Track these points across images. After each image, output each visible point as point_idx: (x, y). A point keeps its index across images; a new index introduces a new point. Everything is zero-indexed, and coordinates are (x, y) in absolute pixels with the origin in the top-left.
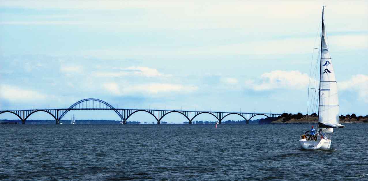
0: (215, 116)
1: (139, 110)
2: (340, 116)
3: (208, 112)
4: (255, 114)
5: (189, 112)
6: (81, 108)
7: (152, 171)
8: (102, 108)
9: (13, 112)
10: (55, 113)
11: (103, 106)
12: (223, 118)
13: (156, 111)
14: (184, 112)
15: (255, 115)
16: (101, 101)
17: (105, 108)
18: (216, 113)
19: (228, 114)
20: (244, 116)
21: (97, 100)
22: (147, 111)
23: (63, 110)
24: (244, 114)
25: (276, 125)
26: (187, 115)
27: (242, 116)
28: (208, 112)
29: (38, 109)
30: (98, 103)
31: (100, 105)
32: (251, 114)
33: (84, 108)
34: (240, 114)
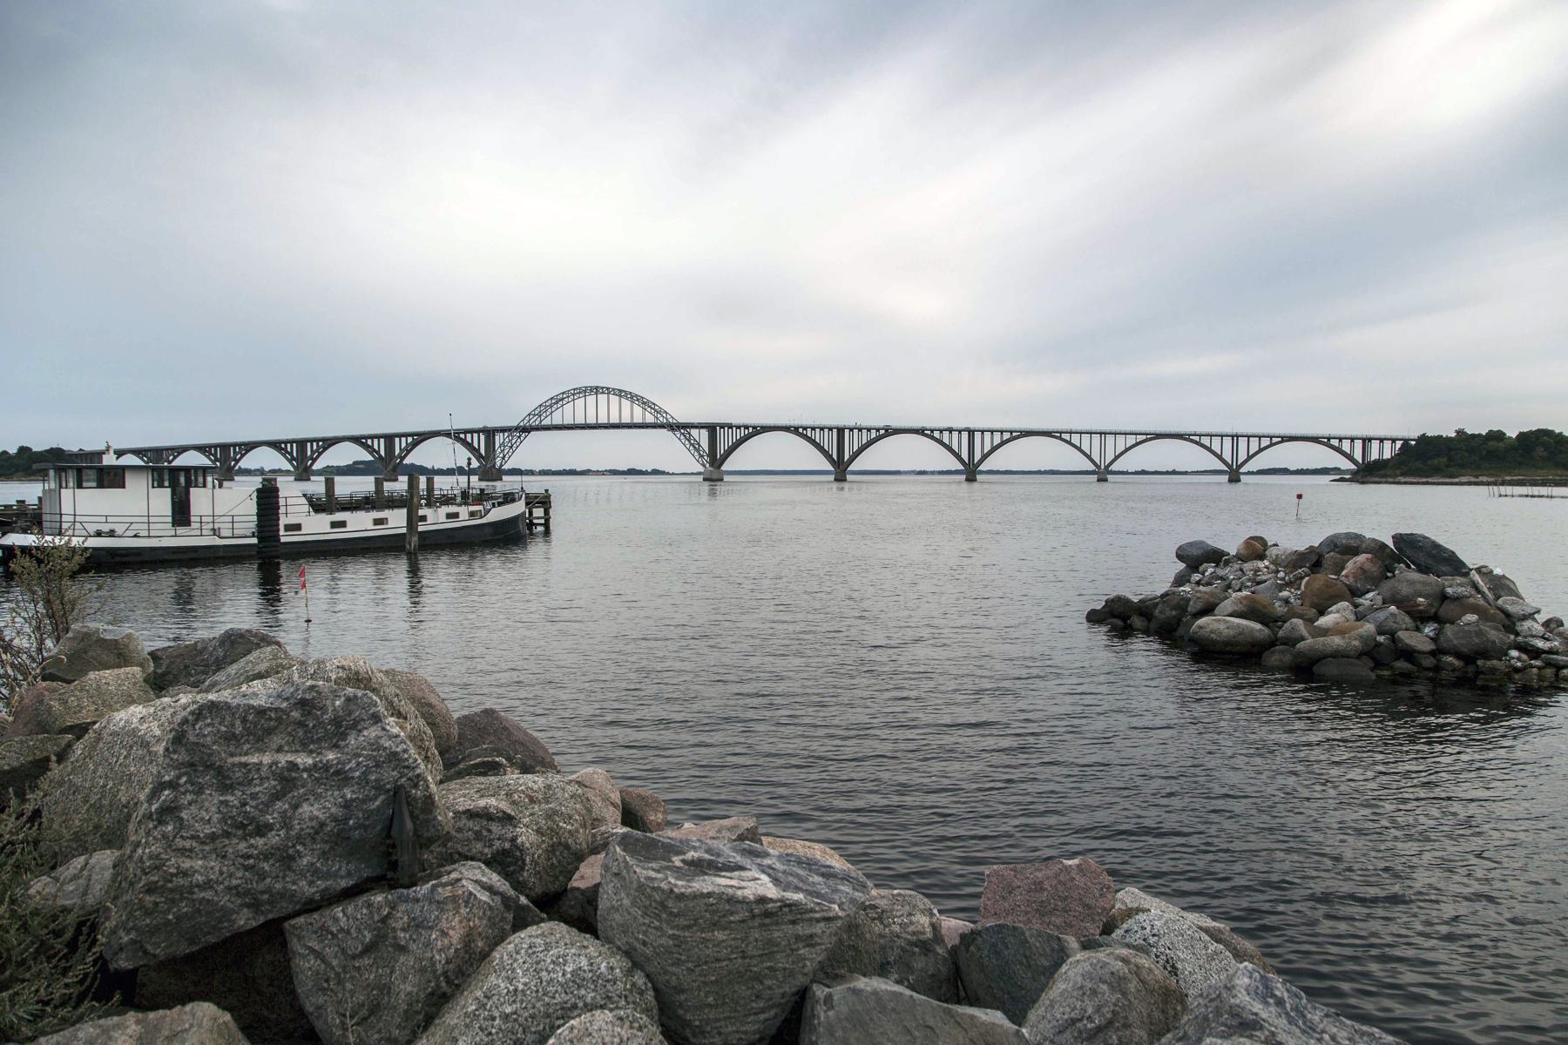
0: (1079, 449)
1: (890, 432)
2: (1089, 628)
3: (1048, 434)
4: (1275, 440)
5: (965, 435)
6: (568, 421)
7: (1365, 712)
8: (626, 419)
9: (1335, 442)
10: (1092, 445)
11: (644, 415)
12: (1117, 458)
13: (983, 432)
14: (946, 434)
15: (1272, 445)
16: (634, 398)
17: (638, 419)
18: (376, 441)
19: (1007, 436)
20: (1085, 448)
21: (621, 393)
22: (1320, 443)
23: (406, 435)
24: (1086, 437)
25: (681, 618)
26: (955, 447)
27: (1209, 449)
28: (1048, 434)
29: (895, 424)
30: (626, 403)
31: (644, 417)
32: (1120, 439)
33: (580, 420)
34: (1197, 438)
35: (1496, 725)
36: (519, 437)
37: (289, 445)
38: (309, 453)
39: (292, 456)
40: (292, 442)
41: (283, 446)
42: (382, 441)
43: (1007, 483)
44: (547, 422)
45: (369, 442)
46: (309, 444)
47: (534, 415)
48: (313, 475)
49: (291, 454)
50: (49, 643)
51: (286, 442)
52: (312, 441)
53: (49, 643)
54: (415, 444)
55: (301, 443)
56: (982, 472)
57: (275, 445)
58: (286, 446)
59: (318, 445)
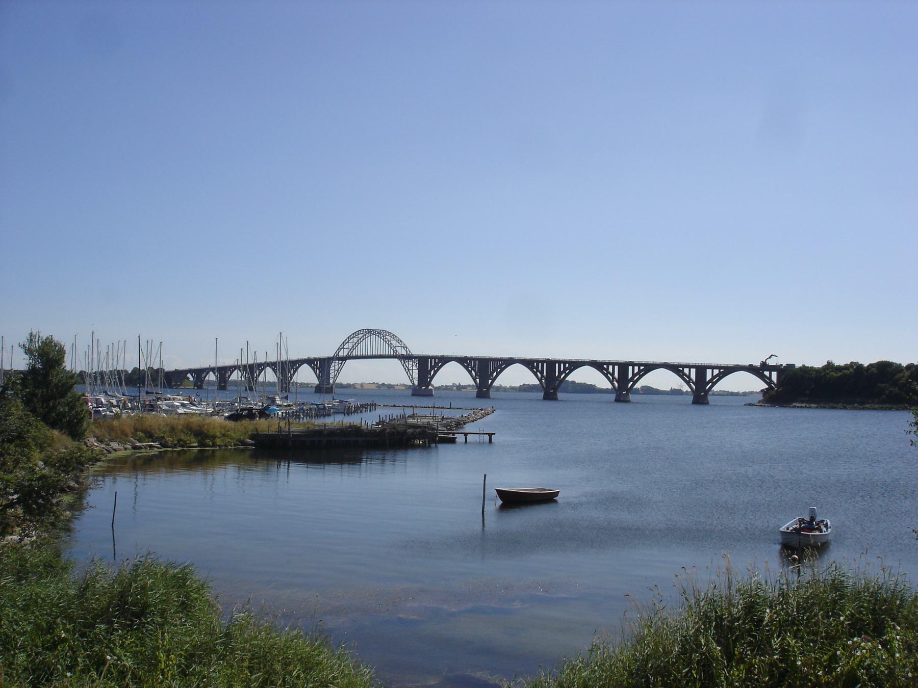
35: (146, 454)
36: (342, 363)
37: (611, 367)
38: (630, 375)
39: (613, 378)
40: (614, 364)
41: (605, 366)
42: (616, 367)
43: (305, 393)
44: (354, 354)
45: (686, 371)
46: (630, 368)
47: (341, 349)
48: (566, 391)
49: (613, 374)
50: (61, 572)
51: (608, 364)
52: (560, 362)
53: (61, 572)
54: (721, 376)
55: (623, 367)
56: (637, 392)
57: (598, 366)
58: (608, 367)
59: (639, 368)
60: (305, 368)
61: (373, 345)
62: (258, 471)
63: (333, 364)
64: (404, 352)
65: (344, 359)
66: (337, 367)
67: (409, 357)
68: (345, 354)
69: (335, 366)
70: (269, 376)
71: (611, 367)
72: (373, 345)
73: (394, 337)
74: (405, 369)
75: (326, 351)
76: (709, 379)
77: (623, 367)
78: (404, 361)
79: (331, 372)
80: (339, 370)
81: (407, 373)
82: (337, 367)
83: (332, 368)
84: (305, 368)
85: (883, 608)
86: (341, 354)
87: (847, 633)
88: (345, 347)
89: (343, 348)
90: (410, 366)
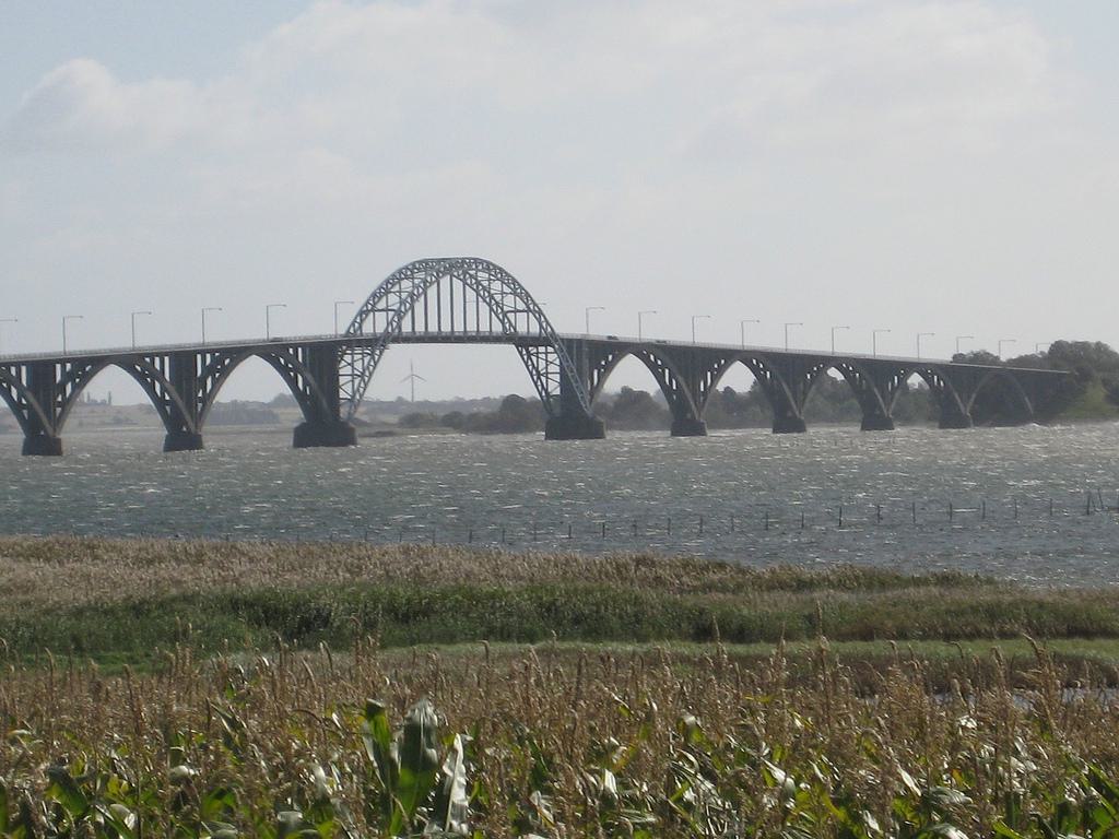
37: (157, 360)
60: (255, 366)
61: (453, 305)
62: (776, 584)
63: (348, 358)
64: (535, 329)
65: (376, 344)
66: (359, 365)
67: (546, 339)
68: (380, 329)
69: (351, 364)
70: (252, 383)
71: (157, 360)
72: (453, 305)
73: (489, 267)
74: (531, 373)
75: (326, 324)
76: (242, 397)
77: (183, 359)
78: (528, 352)
79: (342, 380)
80: (364, 377)
81: (536, 384)
82: (359, 365)
83: (345, 370)
84: (255, 366)
85: (13, 668)
86: (368, 329)
87: (713, 792)
88: (379, 306)
89: (373, 310)
90: (542, 364)
